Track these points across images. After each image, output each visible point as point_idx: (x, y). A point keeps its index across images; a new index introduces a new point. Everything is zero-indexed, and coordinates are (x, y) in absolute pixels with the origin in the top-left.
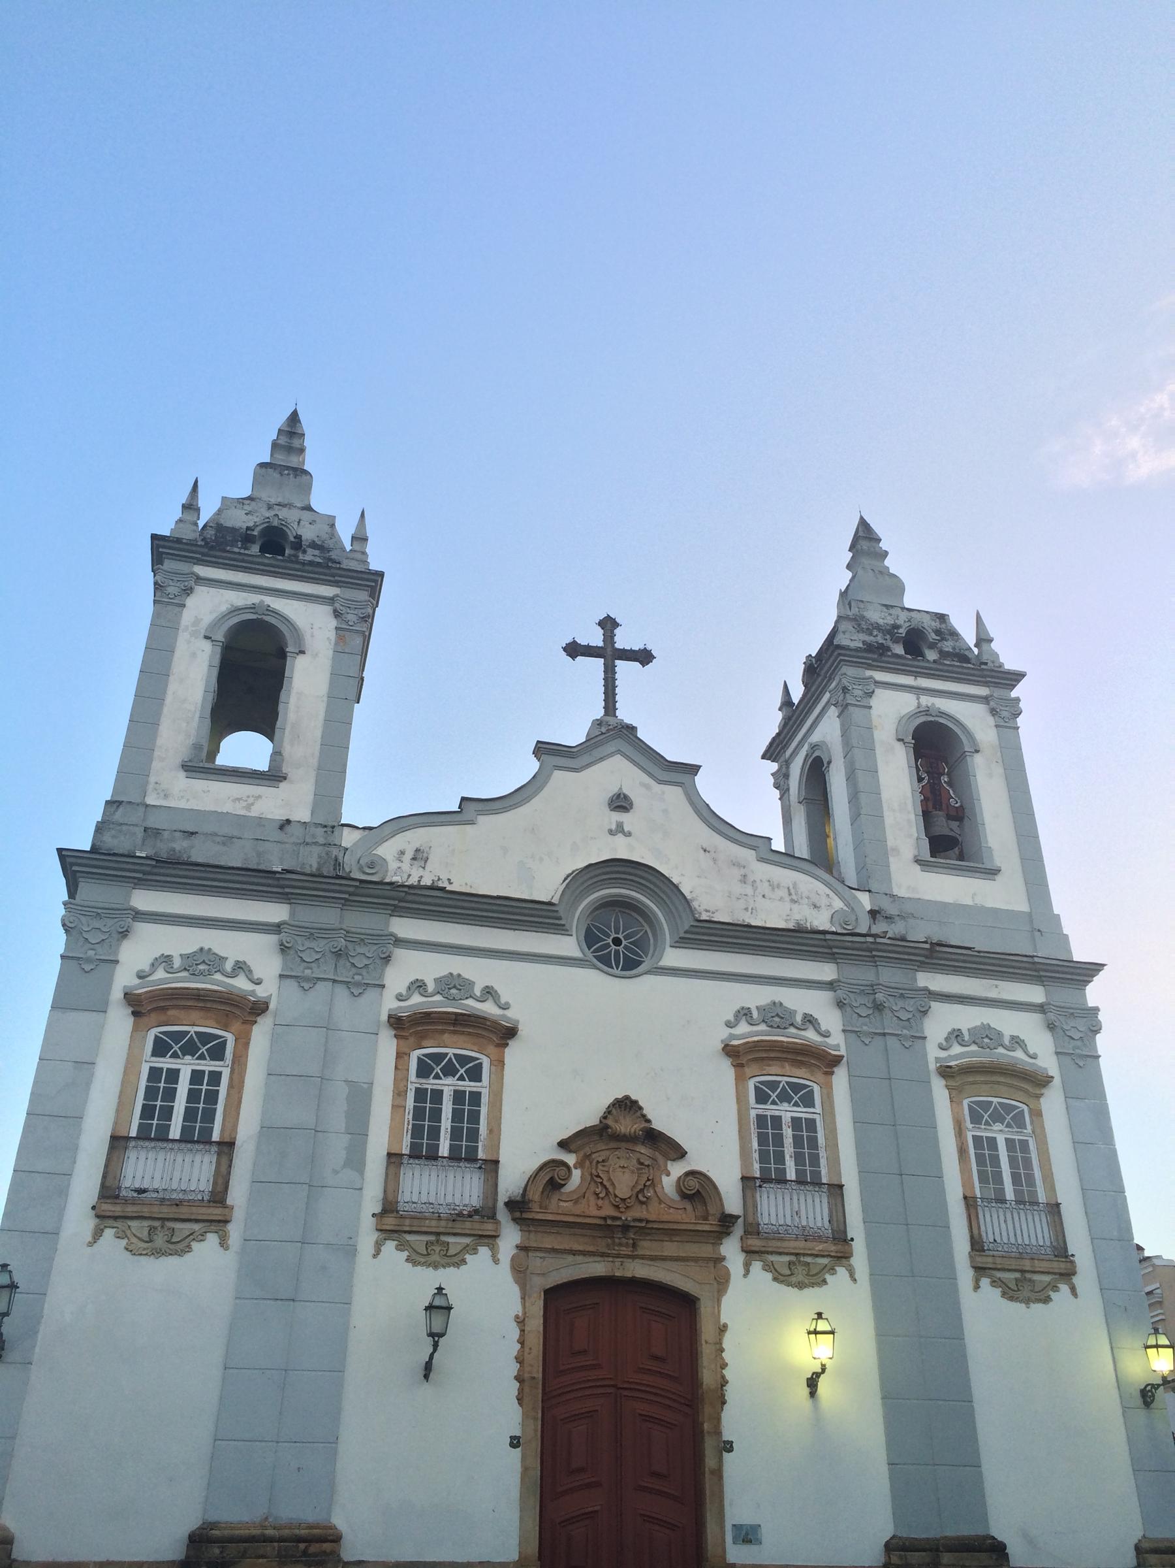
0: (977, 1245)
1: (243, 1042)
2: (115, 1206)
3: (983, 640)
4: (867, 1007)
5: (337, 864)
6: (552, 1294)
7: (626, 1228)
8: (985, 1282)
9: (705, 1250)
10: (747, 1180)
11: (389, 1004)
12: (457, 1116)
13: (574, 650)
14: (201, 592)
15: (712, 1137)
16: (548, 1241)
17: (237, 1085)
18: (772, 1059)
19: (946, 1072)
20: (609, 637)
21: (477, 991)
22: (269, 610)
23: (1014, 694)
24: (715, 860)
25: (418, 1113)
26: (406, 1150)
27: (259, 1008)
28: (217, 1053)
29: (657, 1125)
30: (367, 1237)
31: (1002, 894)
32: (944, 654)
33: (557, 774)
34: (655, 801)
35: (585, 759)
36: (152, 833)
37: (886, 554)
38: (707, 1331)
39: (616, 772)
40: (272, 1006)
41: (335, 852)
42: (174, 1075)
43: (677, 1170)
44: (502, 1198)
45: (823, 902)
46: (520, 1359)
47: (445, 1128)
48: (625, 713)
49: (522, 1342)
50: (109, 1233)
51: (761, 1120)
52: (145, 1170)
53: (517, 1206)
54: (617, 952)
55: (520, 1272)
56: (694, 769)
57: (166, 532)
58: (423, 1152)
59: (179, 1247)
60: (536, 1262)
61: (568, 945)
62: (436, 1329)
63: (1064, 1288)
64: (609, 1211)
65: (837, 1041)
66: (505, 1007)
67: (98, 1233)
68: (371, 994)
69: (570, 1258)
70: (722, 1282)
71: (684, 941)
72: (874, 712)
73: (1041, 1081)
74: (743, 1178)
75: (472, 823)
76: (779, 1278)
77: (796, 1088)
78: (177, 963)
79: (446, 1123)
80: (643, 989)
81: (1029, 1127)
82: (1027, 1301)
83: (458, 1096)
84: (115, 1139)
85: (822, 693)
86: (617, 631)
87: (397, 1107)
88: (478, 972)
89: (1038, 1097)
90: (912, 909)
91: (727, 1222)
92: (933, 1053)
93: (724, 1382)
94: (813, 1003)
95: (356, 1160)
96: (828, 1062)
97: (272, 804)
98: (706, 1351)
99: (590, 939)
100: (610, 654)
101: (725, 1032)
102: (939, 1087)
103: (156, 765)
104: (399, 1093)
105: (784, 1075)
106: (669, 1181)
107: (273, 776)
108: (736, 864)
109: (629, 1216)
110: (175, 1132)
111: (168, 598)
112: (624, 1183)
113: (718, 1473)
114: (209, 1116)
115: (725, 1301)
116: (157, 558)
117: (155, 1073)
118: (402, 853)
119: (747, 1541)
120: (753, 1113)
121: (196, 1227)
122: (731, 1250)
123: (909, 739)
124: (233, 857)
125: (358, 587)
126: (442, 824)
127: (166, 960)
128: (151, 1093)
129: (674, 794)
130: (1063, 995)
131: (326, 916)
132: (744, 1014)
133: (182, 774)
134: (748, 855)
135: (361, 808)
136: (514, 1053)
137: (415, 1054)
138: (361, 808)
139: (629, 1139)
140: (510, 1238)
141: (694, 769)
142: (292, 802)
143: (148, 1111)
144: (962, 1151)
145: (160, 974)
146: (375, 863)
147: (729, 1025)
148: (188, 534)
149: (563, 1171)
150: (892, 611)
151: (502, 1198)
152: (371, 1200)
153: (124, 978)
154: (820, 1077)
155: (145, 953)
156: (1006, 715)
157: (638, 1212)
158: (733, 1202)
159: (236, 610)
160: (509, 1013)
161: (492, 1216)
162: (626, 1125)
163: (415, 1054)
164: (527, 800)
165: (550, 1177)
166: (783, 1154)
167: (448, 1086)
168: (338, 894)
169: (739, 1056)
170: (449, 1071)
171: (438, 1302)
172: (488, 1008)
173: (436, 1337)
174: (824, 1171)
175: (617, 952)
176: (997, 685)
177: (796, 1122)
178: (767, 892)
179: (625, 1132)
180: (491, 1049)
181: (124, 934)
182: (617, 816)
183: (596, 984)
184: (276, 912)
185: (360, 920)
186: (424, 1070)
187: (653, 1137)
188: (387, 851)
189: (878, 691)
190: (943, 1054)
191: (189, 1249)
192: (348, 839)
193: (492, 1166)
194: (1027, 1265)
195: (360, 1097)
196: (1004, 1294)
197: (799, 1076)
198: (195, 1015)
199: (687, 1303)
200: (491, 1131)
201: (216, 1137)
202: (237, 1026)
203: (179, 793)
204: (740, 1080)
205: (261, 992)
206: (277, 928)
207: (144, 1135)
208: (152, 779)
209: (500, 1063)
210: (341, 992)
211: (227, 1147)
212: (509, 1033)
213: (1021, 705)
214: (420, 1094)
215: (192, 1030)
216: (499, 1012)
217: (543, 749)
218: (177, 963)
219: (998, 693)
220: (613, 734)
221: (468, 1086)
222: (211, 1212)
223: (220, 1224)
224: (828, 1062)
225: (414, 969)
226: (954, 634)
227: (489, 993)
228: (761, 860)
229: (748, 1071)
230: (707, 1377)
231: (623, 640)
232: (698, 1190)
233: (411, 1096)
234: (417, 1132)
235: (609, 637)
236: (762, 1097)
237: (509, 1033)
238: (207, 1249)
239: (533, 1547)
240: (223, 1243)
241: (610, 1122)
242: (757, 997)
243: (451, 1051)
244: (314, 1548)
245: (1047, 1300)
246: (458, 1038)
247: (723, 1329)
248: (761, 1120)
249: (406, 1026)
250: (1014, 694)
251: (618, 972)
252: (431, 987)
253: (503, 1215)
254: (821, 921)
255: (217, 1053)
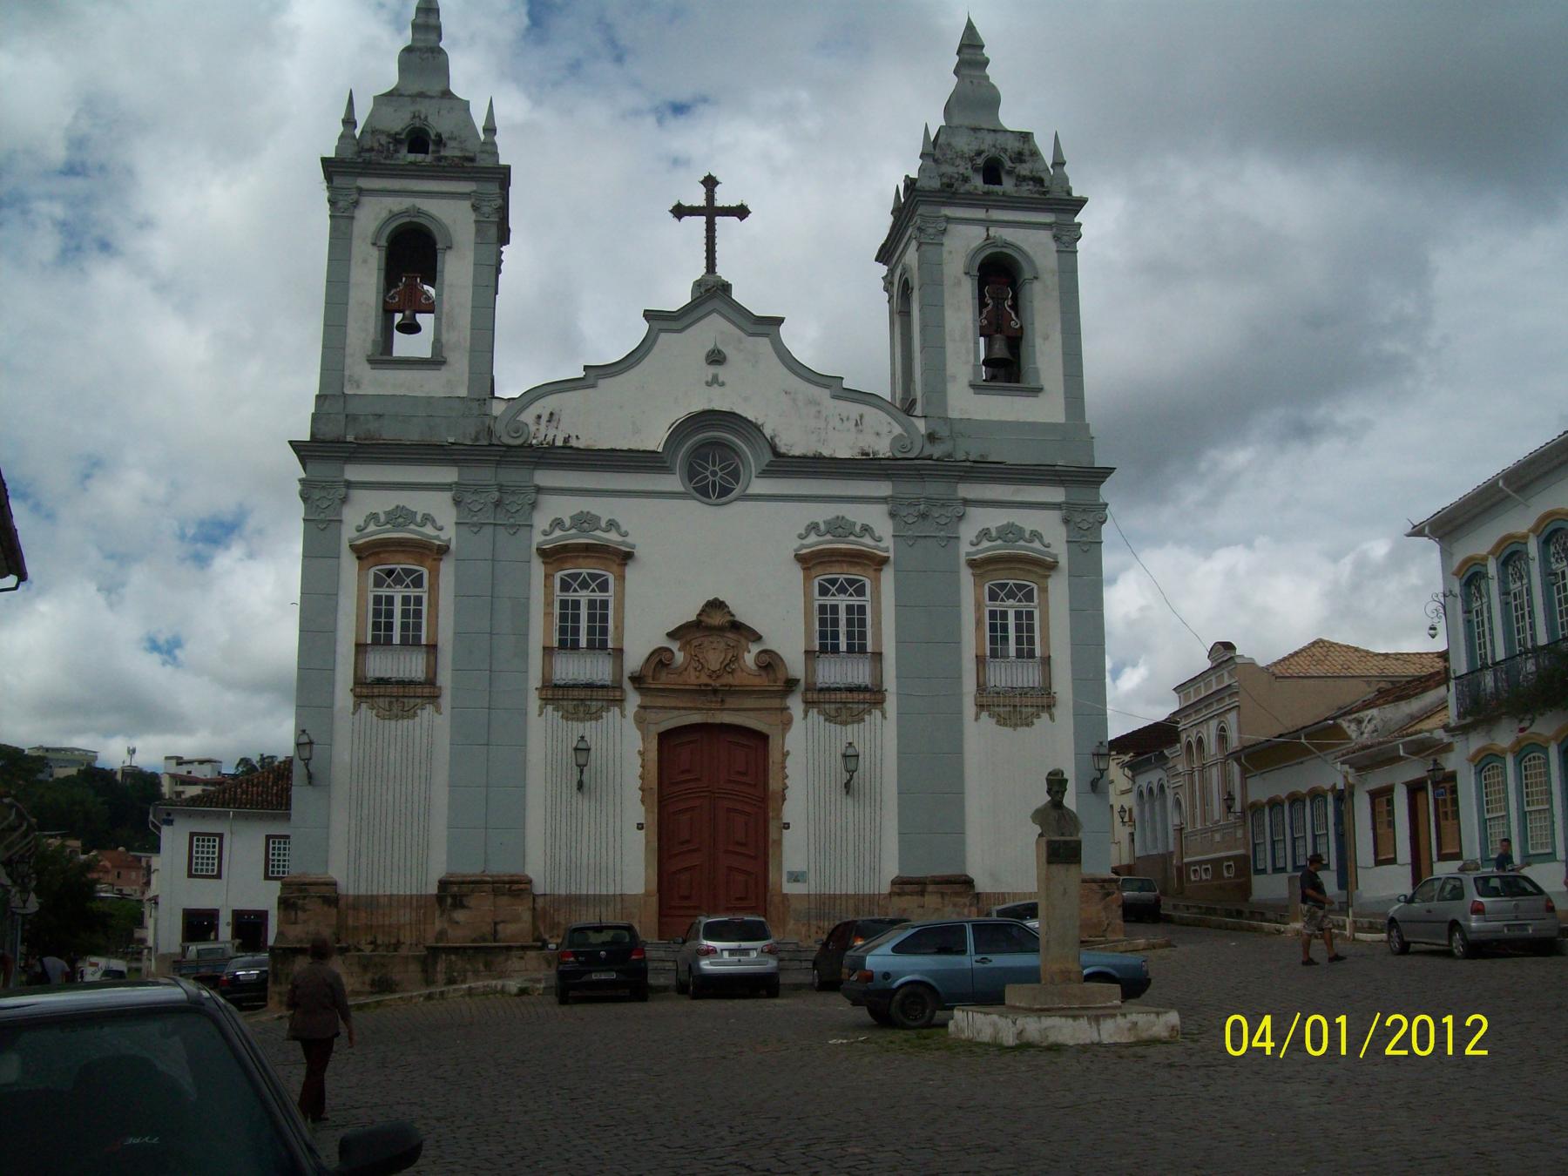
0: (981, 687)
1: (435, 574)
2: (368, 689)
3: (1059, 163)
4: (926, 521)
5: (490, 432)
6: (665, 737)
7: (715, 691)
8: (984, 715)
9: (776, 703)
10: (809, 653)
11: (538, 538)
12: (591, 618)
13: (680, 211)
14: (367, 201)
15: (781, 619)
16: (659, 702)
17: (434, 604)
18: (834, 564)
19: (973, 564)
20: (710, 197)
21: (603, 524)
22: (419, 212)
23: (1077, 220)
24: (794, 400)
25: (563, 618)
26: (556, 644)
27: (443, 550)
28: (418, 582)
29: (741, 618)
30: (534, 702)
31: (1046, 409)
32: (1021, 179)
33: (663, 335)
34: (745, 351)
35: (686, 321)
36: (351, 418)
37: (986, 62)
38: (774, 756)
39: (713, 330)
40: (453, 546)
41: (487, 421)
42: (390, 600)
43: (755, 649)
44: (626, 674)
45: (884, 429)
46: (642, 777)
47: (582, 628)
48: (722, 271)
49: (643, 766)
50: (364, 706)
51: (822, 608)
52: (381, 665)
53: (637, 680)
54: (714, 483)
55: (640, 721)
56: (779, 321)
57: (332, 155)
58: (568, 644)
59: (409, 713)
60: (651, 716)
61: (673, 482)
62: (581, 761)
63: (1045, 716)
64: (704, 679)
65: (449, 534)
66: (626, 535)
67: (357, 707)
68: (523, 532)
69: (676, 713)
70: (787, 723)
71: (766, 473)
72: (946, 249)
73: (1052, 566)
74: (806, 652)
75: (593, 386)
76: (829, 719)
77: (851, 582)
78: (382, 518)
79: (584, 624)
80: (735, 514)
81: (1036, 600)
82: (1015, 726)
83: (592, 604)
84: (358, 645)
85: (906, 228)
86: (717, 189)
87: (548, 615)
88: (602, 508)
89: (1047, 577)
90: (962, 428)
91: (791, 684)
92: (965, 548)
93: (785, 787)
94: (872, 518)
95: (524, 655)
96: (880, 562)
97: (431, 384)
98: (773, 769)
99: (691, 474)
100: (711, 212)
101: (797, 543)
102: (966, 576)
103: (348, 361)
104: (549, 604)
105: (842, 574)
106: (749, 659)
107: (436, 362)
108: (811, 402)
109: (717, 684)
110: (397, 639)
111: (342, 211)
112: (714, 659)
113: (779, 843)
114: (418, 627)
115: (788, 736)
116: (329, 176)
117: (377, 600)
118: (539, 417)
119: (796, 880)
120: (816, 604)
121: (419, 701)
122: (795, 704)
123: (976, 273)
124: (413, 435)
125: (489, 180)
126: (575, 389)
127: (374, 517)
128: (377, 613)
129: (764, 344)
130: (1081, 495)
131: (484, 474)
132: (814, 527)
133: (368, 366)
134: (823, 394)
135: (511, 381)
136: (631, 572)
137: (558, 575)
138: (511, 381)
139: (720, 629)
140: (633, 700)
141: (779, 321)
142: (451, 382)
143: (376, 626)
144: (979, 622)
145: (372, 528)
146: (520, 428)
147: (801, 537)
148: (349, 154)
149: (668, 655)
150: (979, 135)
151: (626, 674)
152: (535, 680)
153: (348, 533)
154: (871, 573)
155: (362, 513)
156: (1067, 237)
157: (727, 679)
158: (795, 664)
159: (393, 216)
160: (629, 540)
161: (620, 687)
162: (717, 619)
163: (558, 575)
164: (638, 361)
165: (660, 659)
166: (837, 633)
167: (584, 596)
168: (500, 453)
169: (808, 561)
170: (584, 585)
171: (582, 745)
172: (613, 537)
173: (581, 767)
174: (869, 642)
175: (714, 483)
176: (1063, 211)
177: (850, 609)
178: (838, 424)
179: (715, 625)
180: (615, 568)
181: (344, 500)
182: (713, 370)
183: (694, 509)
184: (449, 475)
185: (510, 476)
186: (565, 586)
187: (736, 626)
188: (528, 417)
189: (951, 227)
190: (974, 549)
191: (415, 715)
192: (497, 409)
193: (619, 652)
194: (1017, 701)
195: (522, 608)
196: (998, 722)
197: (855, 573)
198: (400, 557)
199: (761, 739)
200: (616, 628)
201: (424, 641)
202: (429, 562)
203: (372, 383)
204: (808, 579)
205: (444, 536)
206: (884, 500)
207: (376, 641)
208: (347, 373)
209: (621, 578)
210: (502, 534)
211: (432, 648)
212: (625, 557)
213: (1082, 230)
214: (564, 604)
215: (399, 567)
216: (436, 533)
217: (649, 315)
218: (382, 518)
219: (1064, 217)
220: (712, 293)
221: (598, 596)
222: (425, 691)
223: (434, 698)
224: (880, 562)
225: (558, 509)
226: (1035, 154)
227: (612, 524)
228: (834, 397)
229: (813, 572)
230: (774, 785)
231: (722, 200)
232: (770, 662)
233: (557, 605)
234: (563, 631)
235: (710, 197)
236: (824, 591)
237: (625, 557)
238: (427, 714)
239: (654, 886)
240: (438, 710)
241: (703, 618)
242: (823, 513)
243: (584, 571)
244: (515, 887)
245: (1029, 724)
246: (593, 559)
247: (785, 755)
248: (822, 608)
249: (553, 556)
250: (1077, 220)
251: (713, 499)
252: (568, 523)
253: (627, 685)
254: (883, 448)
255: (418, 582)
